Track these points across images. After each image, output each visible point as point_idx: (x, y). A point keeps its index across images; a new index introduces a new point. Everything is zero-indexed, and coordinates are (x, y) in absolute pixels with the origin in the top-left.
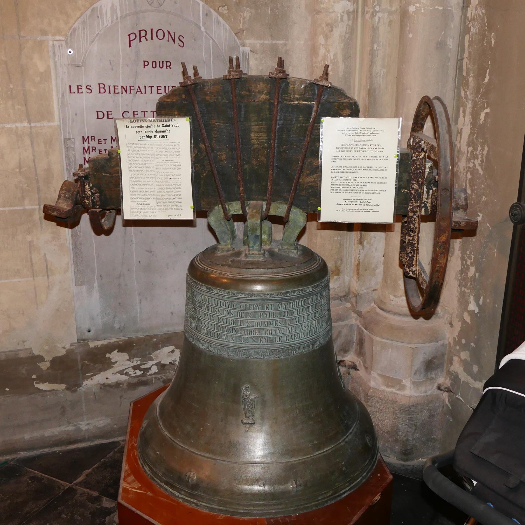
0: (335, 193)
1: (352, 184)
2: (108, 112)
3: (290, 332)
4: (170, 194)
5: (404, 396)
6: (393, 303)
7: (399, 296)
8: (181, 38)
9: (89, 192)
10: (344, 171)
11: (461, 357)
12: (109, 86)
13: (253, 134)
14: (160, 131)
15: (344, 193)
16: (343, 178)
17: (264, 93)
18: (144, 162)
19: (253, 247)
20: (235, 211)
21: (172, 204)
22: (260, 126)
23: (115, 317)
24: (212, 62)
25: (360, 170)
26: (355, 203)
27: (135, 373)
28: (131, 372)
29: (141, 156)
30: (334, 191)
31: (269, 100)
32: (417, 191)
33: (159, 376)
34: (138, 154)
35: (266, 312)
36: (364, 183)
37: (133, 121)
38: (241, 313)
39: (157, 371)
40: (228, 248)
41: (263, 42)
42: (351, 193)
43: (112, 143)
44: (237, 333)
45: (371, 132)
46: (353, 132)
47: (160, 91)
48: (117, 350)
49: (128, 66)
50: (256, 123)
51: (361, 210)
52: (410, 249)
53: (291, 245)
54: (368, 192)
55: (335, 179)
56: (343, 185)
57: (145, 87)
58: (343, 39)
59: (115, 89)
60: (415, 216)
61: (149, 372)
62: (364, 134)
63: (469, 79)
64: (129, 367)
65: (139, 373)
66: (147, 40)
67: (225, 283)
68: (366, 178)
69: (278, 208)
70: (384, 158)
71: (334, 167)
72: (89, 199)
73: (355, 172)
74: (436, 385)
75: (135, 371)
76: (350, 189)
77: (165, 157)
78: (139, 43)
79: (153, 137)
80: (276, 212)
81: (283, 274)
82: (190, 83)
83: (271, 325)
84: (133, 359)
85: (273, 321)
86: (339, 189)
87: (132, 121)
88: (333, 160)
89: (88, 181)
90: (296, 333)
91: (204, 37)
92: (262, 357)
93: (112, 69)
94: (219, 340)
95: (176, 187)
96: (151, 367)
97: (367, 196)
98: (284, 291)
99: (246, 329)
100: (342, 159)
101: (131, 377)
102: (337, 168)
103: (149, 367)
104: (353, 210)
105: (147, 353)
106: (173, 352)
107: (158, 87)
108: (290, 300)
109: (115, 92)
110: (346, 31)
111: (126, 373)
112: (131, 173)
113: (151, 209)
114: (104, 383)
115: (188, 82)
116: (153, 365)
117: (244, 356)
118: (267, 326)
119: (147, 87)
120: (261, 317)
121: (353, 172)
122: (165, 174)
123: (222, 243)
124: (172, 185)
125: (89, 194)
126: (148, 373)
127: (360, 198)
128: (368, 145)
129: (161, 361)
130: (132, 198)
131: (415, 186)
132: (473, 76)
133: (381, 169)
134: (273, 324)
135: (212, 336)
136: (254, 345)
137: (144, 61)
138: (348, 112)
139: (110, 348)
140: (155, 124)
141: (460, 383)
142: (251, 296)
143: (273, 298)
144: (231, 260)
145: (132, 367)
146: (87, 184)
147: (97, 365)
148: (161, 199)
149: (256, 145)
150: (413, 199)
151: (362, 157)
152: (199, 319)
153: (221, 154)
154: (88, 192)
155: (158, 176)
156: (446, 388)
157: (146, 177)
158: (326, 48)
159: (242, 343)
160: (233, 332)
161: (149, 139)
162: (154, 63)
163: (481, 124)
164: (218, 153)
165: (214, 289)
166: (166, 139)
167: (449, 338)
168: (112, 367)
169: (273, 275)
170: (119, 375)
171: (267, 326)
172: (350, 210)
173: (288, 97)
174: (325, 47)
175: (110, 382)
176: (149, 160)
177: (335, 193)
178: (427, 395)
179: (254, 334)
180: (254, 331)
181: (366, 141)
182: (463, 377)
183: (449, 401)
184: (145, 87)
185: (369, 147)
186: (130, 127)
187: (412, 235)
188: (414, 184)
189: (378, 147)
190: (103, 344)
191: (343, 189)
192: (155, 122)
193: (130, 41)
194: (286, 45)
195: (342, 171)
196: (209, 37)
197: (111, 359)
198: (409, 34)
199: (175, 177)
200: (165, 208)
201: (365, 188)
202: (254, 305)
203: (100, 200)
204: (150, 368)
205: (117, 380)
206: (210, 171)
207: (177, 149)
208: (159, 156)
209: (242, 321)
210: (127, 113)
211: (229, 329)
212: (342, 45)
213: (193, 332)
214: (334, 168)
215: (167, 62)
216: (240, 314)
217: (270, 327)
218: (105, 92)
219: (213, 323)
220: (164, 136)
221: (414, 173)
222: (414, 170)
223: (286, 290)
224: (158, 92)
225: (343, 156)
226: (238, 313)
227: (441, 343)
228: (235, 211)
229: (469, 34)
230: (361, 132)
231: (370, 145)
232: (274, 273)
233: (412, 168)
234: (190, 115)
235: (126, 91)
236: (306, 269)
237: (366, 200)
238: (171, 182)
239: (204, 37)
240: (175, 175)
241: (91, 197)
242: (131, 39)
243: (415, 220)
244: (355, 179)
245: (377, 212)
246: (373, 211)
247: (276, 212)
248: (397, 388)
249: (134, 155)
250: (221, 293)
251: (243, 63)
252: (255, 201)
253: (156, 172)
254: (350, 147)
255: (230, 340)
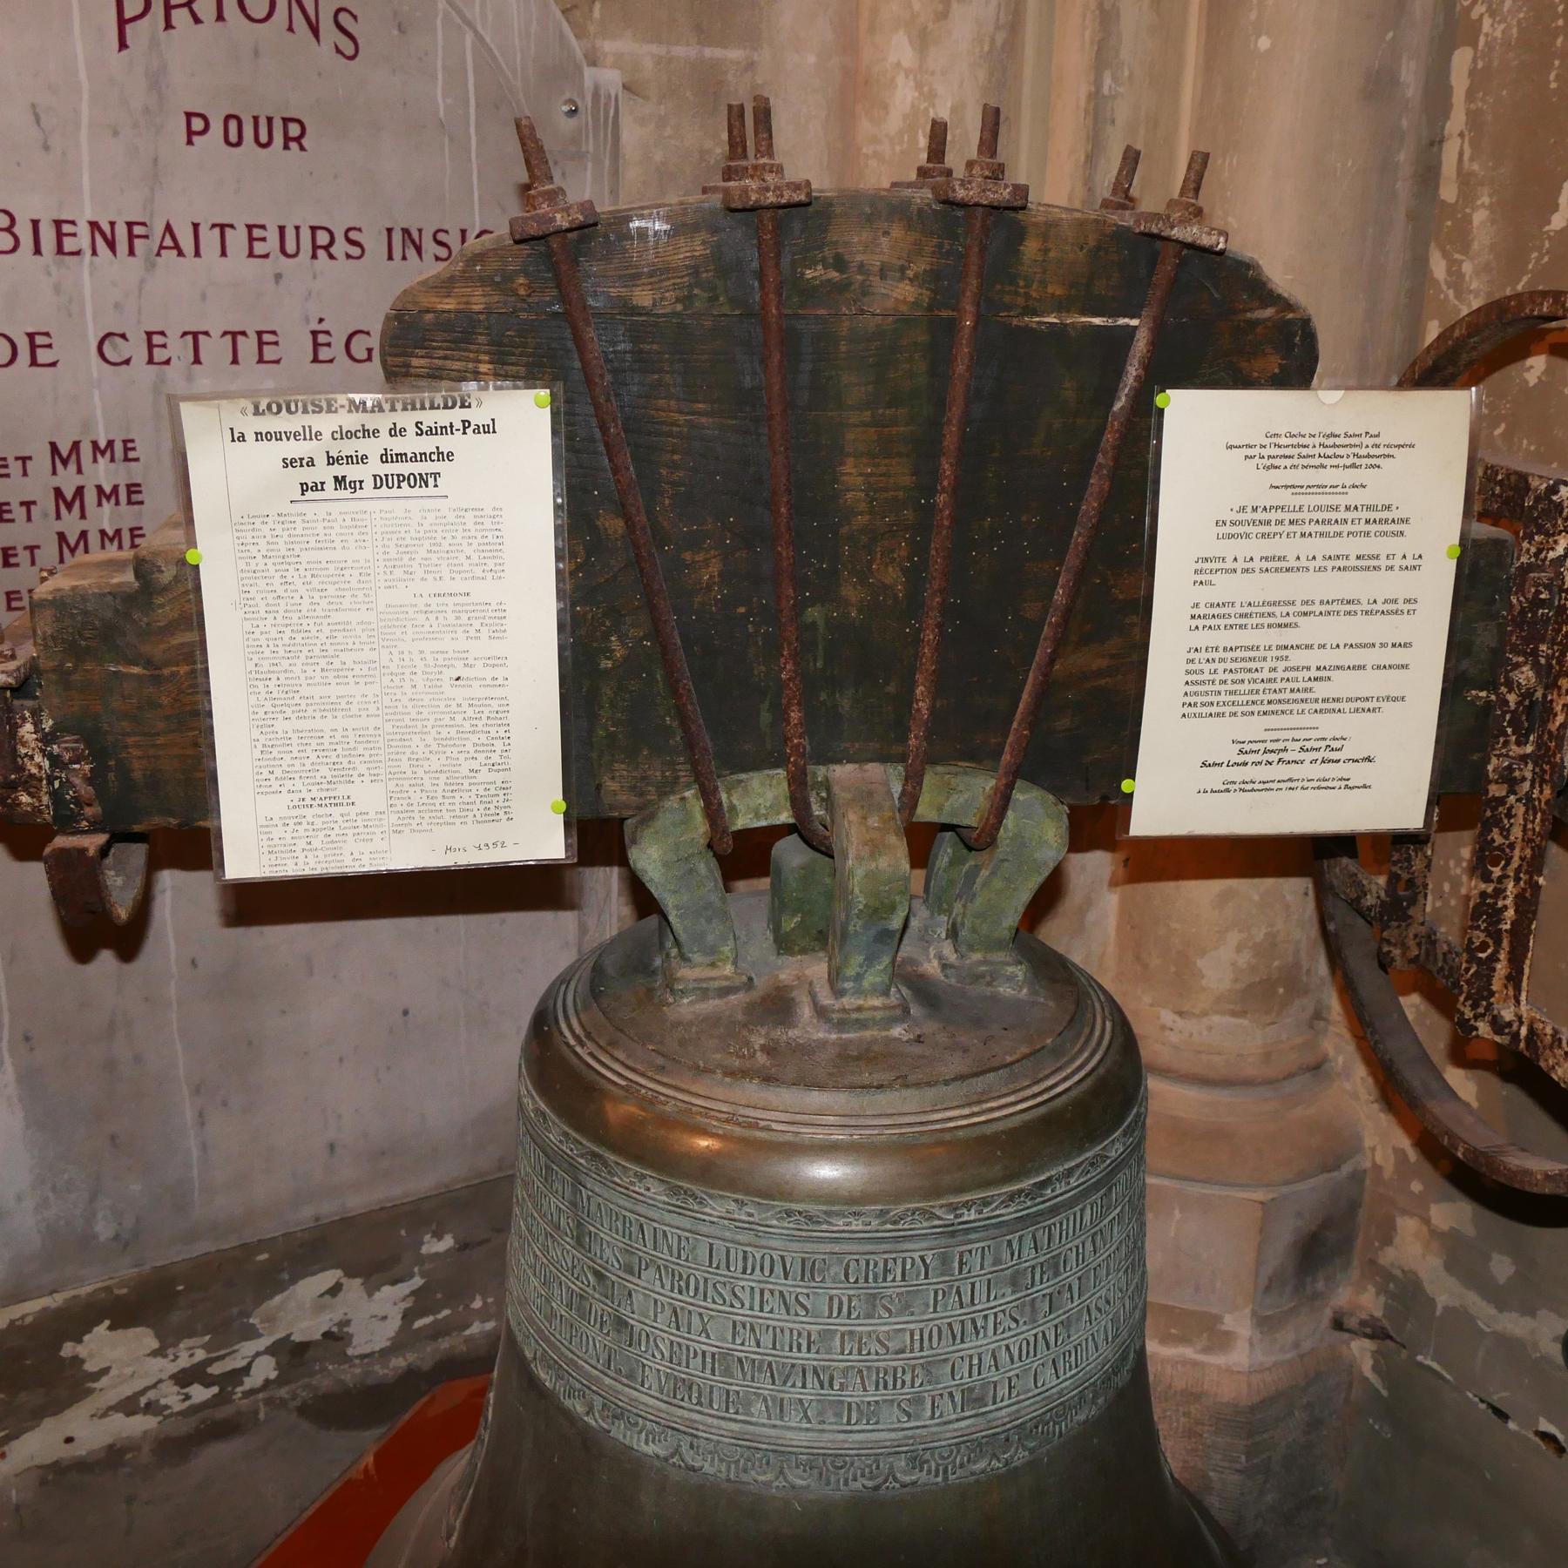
0: (1201, 715)
1: (1273, 675)
2: (31, 336)
3: (1048, 1349)
4: (455, 750)
5: (1229, 1371)
6: (1174, 1038)
7: (1197, 1011)
8: (344, 18)
9: (38, 758)
10: (1243, 621)
11: (1434, 1221)
12: (35, 224)
13: (849, 467)
14: (401, 457)
15: (1235, 714)
16: (1238, 654)
17: (910, 273)
18: (324, 603)
19: (858, 978)
20: (757, 816)
21: (465, 795)
22: (884, 426)
23: (93, 1198)
24: (472, 130)
25: (1305, 614)
26: (1275, 753)
27: (188, 1397)
28: (171, 1398)
29: (308, 574)
30: (1198, 710)
31: (930, 308)
32: (1529, 694)
33: (283, 1392)
34: (291, 568)
35: (956, 1284)
36: (1318, 669)
37: (269, 407)
38: (845, 1300)
39: (276, 1373)
40: (727, 978)
41: (668, 52)
42: (1265, 713)
43: (54, 472)
44: (826, 1385)
45: (1363, 452)
46: (1288, 452)
47: (259, 248)
48: (107, 1323)
49: (116, 133)
50: (867, 415)
51: (1300, 784)
52: (1482, 931)
53: (999, 945)
54: (1331, 706)
55: (1204, 655)
56: (1233, 682)
57: (196, 226)
58: (986, 48)
59: (60, 236)
60: (1512, 798)
61: (242, 1383)
62: (1335, 462)
63: (1470, 216)
64: (160, 1381)
65: (200, 1393)
66: (197, 20)
67: (1320, 1558)
68: (1328, 646)
69: (950, 790)
70: (1404, 563)
71: (1202, 605)
72: (39, 789)
73: (1286, 626)
74: (1328, 1313)
75: (185, 1391)
76: (1261, 697)
77: (430, 577)
78: (163, 35)
79: (368, 484)
80: (940, 809)
81: (1012, 1099)
82: (566, 225)
83: (977, 1333)
84: (175, 1345)
85: (986, 1317)
86: (1215, 699)
87: (263, 406)
88: (1199, 578)
89: (29, 703)
90: (1067, 1348)
91: (439, 22)
92: (937, 1476)
93: (46, 148)
94: (735, 1421)
95: (484, 716)
96: (249, 1365)
97: (1329, 726)
98: (1032, 1182)
99: (869, 1368)
100: (1239, 571)
101: (171, 1415)
102: (1216, 611)
103: (243, 1363)
104: (1267, 786)
105: (235, 1311)
106: (335, 1290)
107: (250, 227)
108: (1054, 1211)
109: (60, 250)
110: (998, 19)
111: (148, 1405)
112: (256, 658)
113: (359, 823)
114: (56, 1462)
115: (558, 216)
116: (258, 1354)
117: (858, 1485)
118: (962, 1341)
119: (203, 230)
120: (935, 1307)
121: (1280, 626)
122: (429, 658)
123: (697, 958)
124: (465, 707)
125: (38, 764)
126: (239, 1389)
127: (1297, 734)
128: (1348, 508)
129: (289, 1336)
130: (266, 775)
131: (1525, 675)
132: (1491, 204)
133: (1393, 608)
134: (984, 1328)
135: (699, 1403)
136: (903, 1429)
137: (189, 115)
138: (1273, 363)
139: (77, 1320)
140: (383, 422)
141: (1434, 1312)
142: (895, 1223)
143: (988, 1218)
144: (758, 1041)
145: (173, 1377)
146: (24, 719)
147: (23, 1397)
148: (409, 774)
149: (861, 513)
150: (1509, 730)
151: (1319, 558)
152: (621, 1324)
153: (700, 557)
154: (32, 758)
155: (393, 668)
156: (1363, 1323)
157: (331, 674)
158: (919, 86)
159: (849, 1428)
160: (809, 1385)
161: (347, 494)
162: (233, 125)
163: (1531, 384)
164: (687, 556)
165: (711, 1197)
166: (431, 490)
167: (1373, 1149)
168: (90, 1391)
169: (976, 1109)
170: (120, 1416)
171: (962, 1341)
172: (1256, 786)
173: (1017, 294)
174: (915, 79)
175: (79, 1450)
176: (348, 594)
177: (1201, 715)
178: (1301, 1357)
179: (904, 1382)
180: (904, 1372)
181: (1339, 489)
182: (1445, 1292)
183: (1375, 1368)
184: (196, 226)
185: (1350, 515)
186: (250, 437)
187: (1497, 872)
188: (1517, 666)
189: (1385, 515)
190: (44, 1309)
191: (1233, 698)
192: (381, 410)
193: (122, 22)
194: (750, 66)
195: (1232, 621)
196: (459, 21)
197: (83, 1361)
198: (1259, 36)
199: (479, 671)
200: (426, 815)
201: (1321, 690)
202: (909, 1261)
203: (101, 794)
204: (246, 1370)
205: (108, 1440)
206: (643, 638)
207: (490, 539)
208: (398, 573)
209: (851, 1333)
210: (118, 340)
211: (784, 1374)
212: (982, 75)
213: (566, 1357)
214: (1202, 611)
215: (286, 121)
216: (841, 1304)
217: (973, 1344)
218: (14, 250)
219: (704, 1347)
220: (423, 480)
221: (1519, 621)
222: (1523, 612)
223: (1038, 1175)
224: (251, 248)
225: (1241, 560)
226: (831, 1299)
227: (1346, 1169)
228: (757, 816)
229: (1474, 45)
230: (1323, 451)
231: (1356, 508)
232: (975, 1098)
233: (1515, 601)
234: (555, 378)
235: (111, 245)
236: (1081, 1052)
237: (1324, 739)
238: (459, 693)
239: (439, 22)
240: (479, 663)
241: (50, 781)
242: (128, 14)
243: (1509, 815)
244: (1284, 653)
245: (1365, 787)
246: (1350, 784)
247: (940, 809)
248: (1199, 1347)
249: (272, 573)
250: (751, 1215)
251: (594, 136)
252: (850, 767)
253: (385, 652)
254: (1273, 516)
255: (794, 1419)
